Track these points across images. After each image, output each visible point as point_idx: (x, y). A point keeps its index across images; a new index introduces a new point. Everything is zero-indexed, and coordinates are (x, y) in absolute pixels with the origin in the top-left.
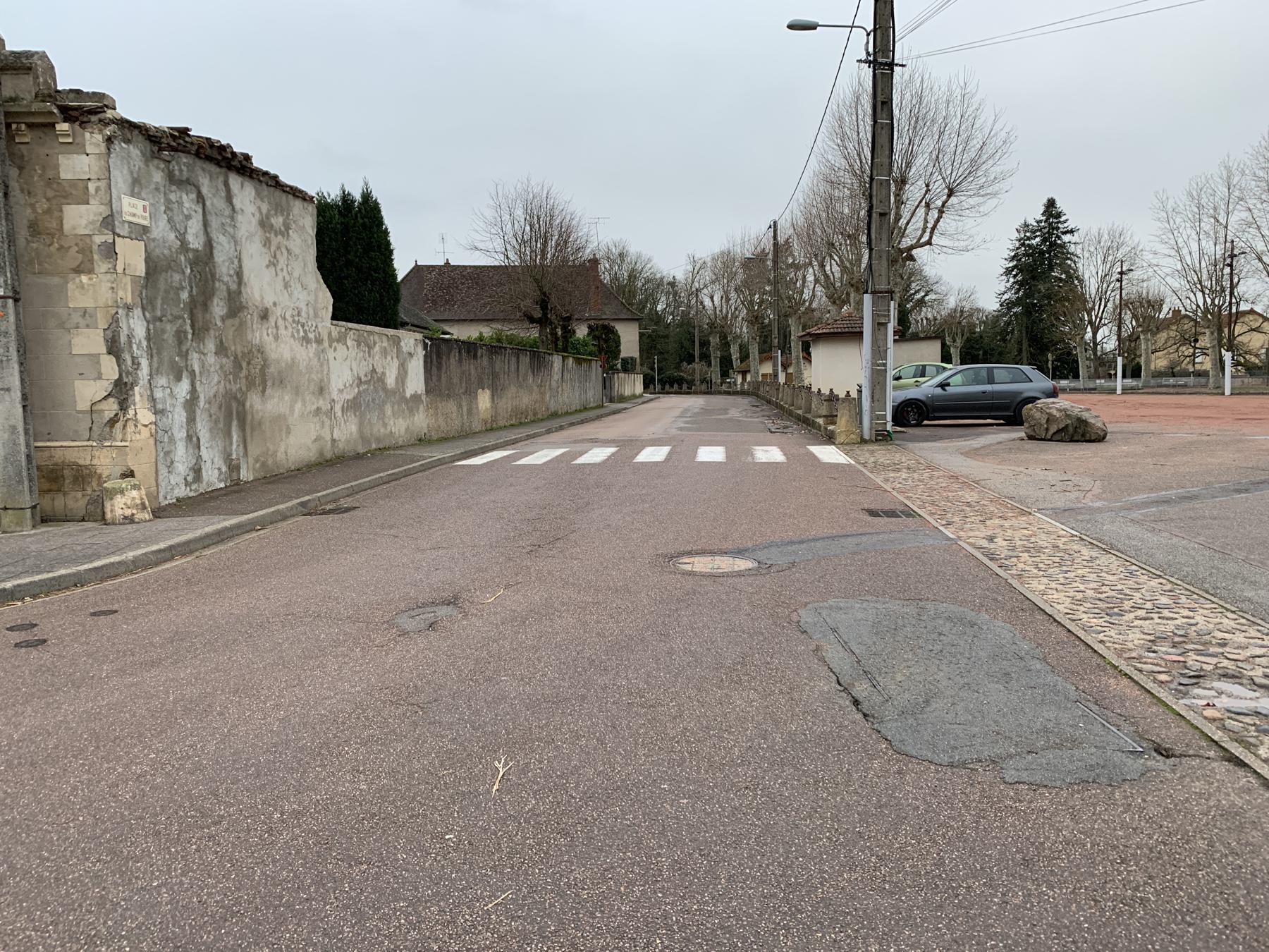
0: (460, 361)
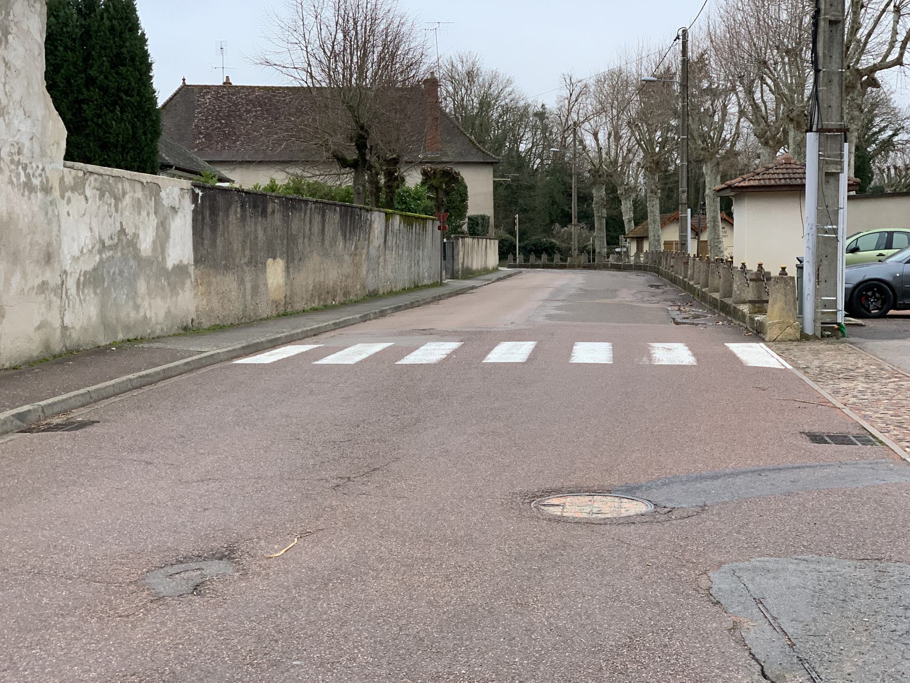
0: (243, 218)
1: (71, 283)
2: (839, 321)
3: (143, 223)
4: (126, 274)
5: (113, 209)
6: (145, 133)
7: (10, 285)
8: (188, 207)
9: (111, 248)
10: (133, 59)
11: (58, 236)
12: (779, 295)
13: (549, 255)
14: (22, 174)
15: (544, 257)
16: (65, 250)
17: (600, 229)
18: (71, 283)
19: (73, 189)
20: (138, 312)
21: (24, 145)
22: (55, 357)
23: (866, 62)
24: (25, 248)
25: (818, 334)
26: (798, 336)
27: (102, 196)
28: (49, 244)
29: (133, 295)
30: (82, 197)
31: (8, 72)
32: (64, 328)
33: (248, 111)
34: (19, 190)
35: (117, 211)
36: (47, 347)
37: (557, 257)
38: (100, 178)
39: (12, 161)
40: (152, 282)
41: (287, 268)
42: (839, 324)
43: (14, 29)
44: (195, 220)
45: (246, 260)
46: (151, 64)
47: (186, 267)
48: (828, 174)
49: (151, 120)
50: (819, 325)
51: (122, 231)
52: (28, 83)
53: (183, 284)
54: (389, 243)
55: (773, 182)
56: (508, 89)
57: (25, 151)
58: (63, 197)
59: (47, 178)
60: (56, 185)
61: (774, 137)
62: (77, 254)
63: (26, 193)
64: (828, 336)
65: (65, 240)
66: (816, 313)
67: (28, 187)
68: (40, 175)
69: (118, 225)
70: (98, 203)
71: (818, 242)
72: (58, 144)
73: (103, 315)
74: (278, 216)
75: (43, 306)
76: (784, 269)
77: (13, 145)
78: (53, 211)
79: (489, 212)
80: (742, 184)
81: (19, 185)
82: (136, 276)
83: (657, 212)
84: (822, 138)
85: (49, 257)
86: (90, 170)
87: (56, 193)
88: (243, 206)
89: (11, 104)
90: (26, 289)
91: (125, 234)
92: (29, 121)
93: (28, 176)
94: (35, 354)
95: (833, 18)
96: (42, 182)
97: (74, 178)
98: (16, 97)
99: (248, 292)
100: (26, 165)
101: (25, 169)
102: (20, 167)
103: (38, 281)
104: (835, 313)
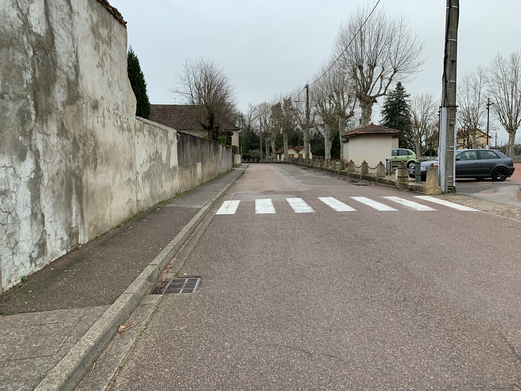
0: (191, 147)
1: (140, 178)
2: (454, 185)
3: (163, 148)
4: (158, 172)
5: (154, 141)
6: (144, 113)
7: (115, 181)
8: (176, 141)
9: (154, 159)
10: (139, 83)
11: (134, 154)
12: (432, 175)
13: (249, 159)
14: (119, 121)
15: (247, 160)
16: (137, 161)
17: (268, 151)
18: (140, 178)
19: (140, 131)
20: (162, 189)
21: (119, 105)
22: (134, 217)
23: (372, 95)
24: (121, 161)
25: (447, 191)
26: (441, 192)
27: (150, 134)
28: (131, 159)
29: (161, 182)
30: (143, 135)
31: (112, 63)
32: (138, 201)
33: (157, 113)
34: (118, 130)
35: (155, 142)
36: (131, 212)
37: (251, 160)
38: (149, 126)
39: (114, 113)
40: (166, 174)
41: (202, 166)
42: (454, 187)
43: (114, 40)
44: (178, 147)
45: (192, 163)
46: (146, 85)
47: (176, 167)
48: (450, 125)
49: (147, 107)
50: (447, 187)
51: (157, 152)
52: (121, 72)
53: (175, 175)
54: (223, 156)
55: (370, 132)
56: (233, 108)
57: (120, 108)
58: (136, 134)
59: (129, 124)
60: (133, 127)
61: (329, 121)
62: (142, 163)
63: (121, 131)
64: (450, 192)
65: (137, 156)
66: (445, 182)
67: (121, 128)
68: (127, 122)
69: (155, 148)
70: (149, 138)
71: (447, 153)
72: (133, 107)
73: (151, 192)
74: (199, 145)
75: (129, 191)
76: (381, 162)
77: (114, 104)
78: (132, 141)
79: (238, 145)
80: (360, 133)
81: (118, 127)
82: (161, 172)
83: (287, 145)
84: (449, 110)
85: (131, 166)
86: (146, 121)
87: (133, 132)
88: (191, 141)
89: (113, 81)
90: (122, 183)
91: (158, 153)
92: (121, 92)
93: (121, 122)
94: (126, 217)
95: (453, 60)
96: (127, 126)
97: (140, 125)
98: (116, 78)
99: (193, 176)
100: (120, 116)
101: (120, 118)
102: (118, 117)
103: (127, 178)
104: (453, 182)
